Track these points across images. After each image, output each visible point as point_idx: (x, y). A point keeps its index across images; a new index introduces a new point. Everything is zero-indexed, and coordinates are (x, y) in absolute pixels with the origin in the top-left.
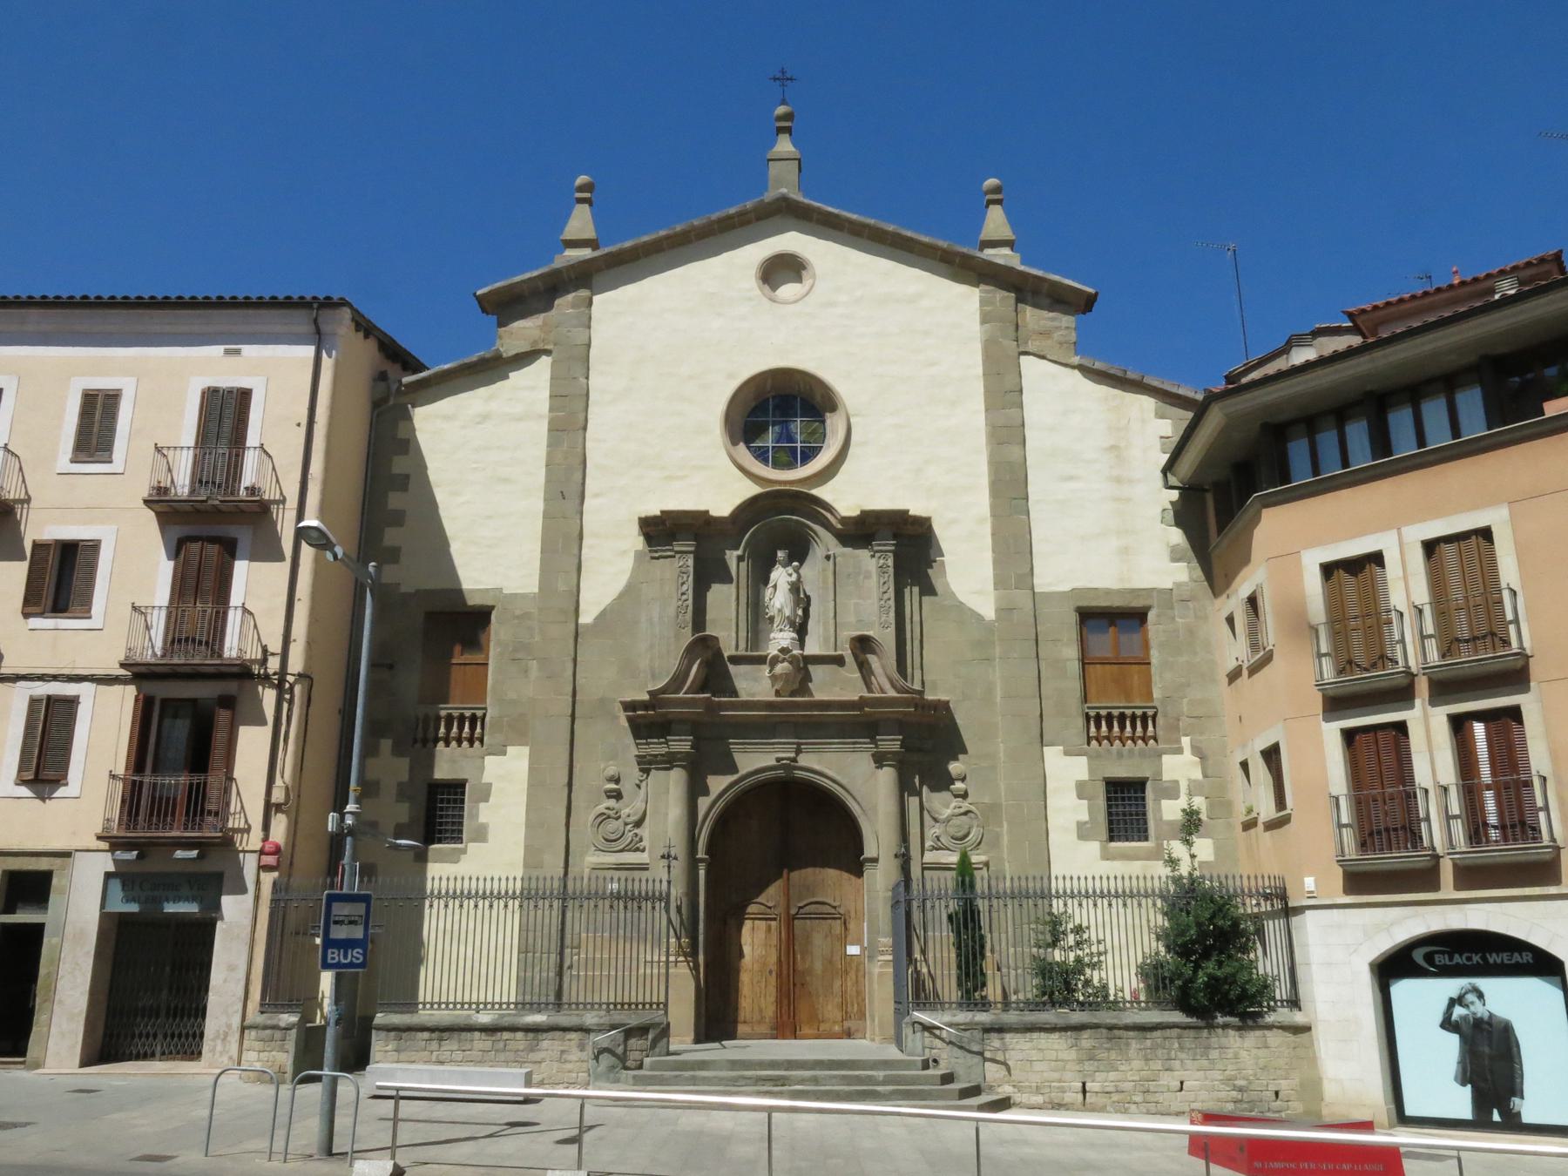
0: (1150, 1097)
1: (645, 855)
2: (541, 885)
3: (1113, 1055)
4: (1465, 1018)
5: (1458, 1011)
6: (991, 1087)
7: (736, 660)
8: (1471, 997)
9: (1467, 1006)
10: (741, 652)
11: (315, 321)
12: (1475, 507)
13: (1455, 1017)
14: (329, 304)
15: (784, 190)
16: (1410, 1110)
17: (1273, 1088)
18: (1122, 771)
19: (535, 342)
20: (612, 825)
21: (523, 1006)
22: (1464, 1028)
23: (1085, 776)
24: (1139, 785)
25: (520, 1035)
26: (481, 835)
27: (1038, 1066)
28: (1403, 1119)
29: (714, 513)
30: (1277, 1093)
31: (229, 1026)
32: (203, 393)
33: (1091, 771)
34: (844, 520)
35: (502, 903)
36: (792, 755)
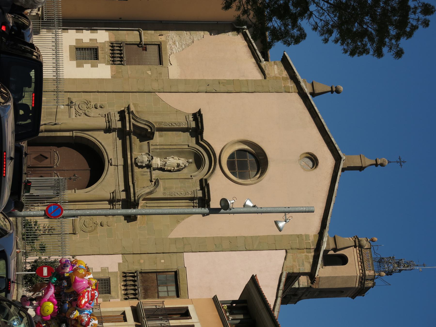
1: (74, 117)
7: (148, 143)
10: (151, 147)
15: (344, 157)
18: (100, 52)
19: (269, 74)
20: (85, 106)
23: (90, 65)
24: (97, 58)
26: (78, 66)
32: (305, 38)
33: (112, 273)
35: (54, 36)
36: (113, 164)
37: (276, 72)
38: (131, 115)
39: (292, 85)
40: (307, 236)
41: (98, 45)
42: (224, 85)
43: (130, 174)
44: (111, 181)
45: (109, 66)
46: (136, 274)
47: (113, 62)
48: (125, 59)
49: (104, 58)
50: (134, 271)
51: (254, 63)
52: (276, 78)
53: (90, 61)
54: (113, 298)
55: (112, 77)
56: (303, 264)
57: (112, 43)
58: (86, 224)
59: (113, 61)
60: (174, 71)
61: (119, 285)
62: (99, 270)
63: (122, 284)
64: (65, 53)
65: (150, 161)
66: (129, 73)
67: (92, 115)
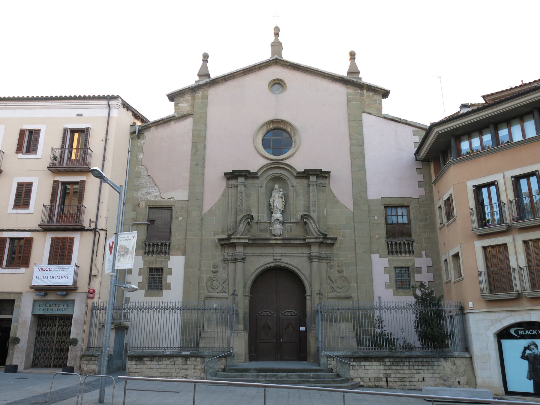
0: (411, 383)
2: (102, 305)
3: (398, 368)
4: (531, 354)
5: (528, 352)
6: (352, 379)
8: (532, 347)
9: (531, 350)
11: (109, 104)
12: (532, 163)
13: (526, 354)
14: (110, 98)
16: (511, 389)
17: (457, 380)
18: (154, 266)
21: (182, 348)
22: (530, 358)
25: (180, 359)
26: (169, 287)
27: (370, 372)
28: (508, 393)
29: (251, 171)
30: (459, 382)
31: (76, 355)
34: (299, 173)
36: (280, 258)
37: (186, 105)
38: (233, 237)
39: (201, 92)
40: (348, 95)
41: (146, 267)
42: (198, 151)
43: (292, 242)
44: (294, 259)
45: (171, 257)
46: (390, 243)
47: (167, 253)
48: (163, 241)
49: (161, 262)
50: (387, 245)
51: (175, 123)
52: (193, 105)
53: (164, 276)
54: (414, 264)
55: (183, 255)
56: (375, 100)
57: (145, 253)
58: (341, 287)
59: (165, 253)
60: (180, 195)
61: (401, 258)
62: (387, 276)
63: (400, 255)
64: (154, 300)
65: (280, 222)
66: (180, 238)
67: (225, 276)
